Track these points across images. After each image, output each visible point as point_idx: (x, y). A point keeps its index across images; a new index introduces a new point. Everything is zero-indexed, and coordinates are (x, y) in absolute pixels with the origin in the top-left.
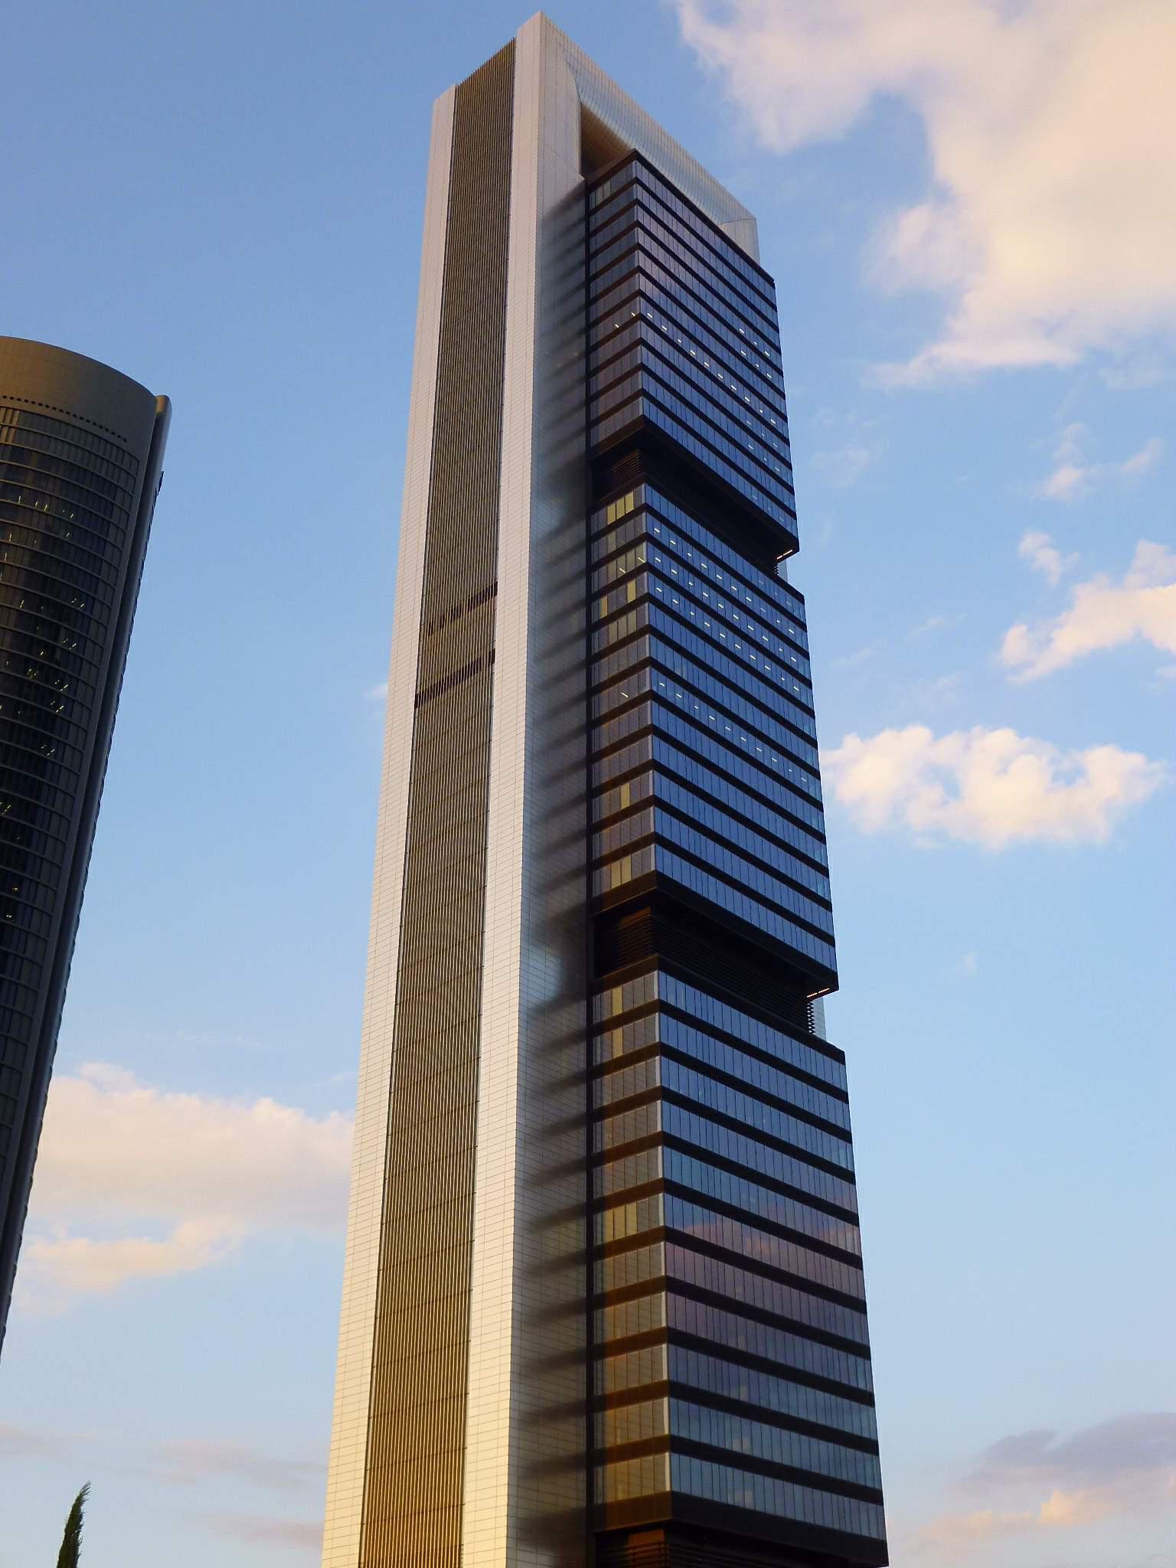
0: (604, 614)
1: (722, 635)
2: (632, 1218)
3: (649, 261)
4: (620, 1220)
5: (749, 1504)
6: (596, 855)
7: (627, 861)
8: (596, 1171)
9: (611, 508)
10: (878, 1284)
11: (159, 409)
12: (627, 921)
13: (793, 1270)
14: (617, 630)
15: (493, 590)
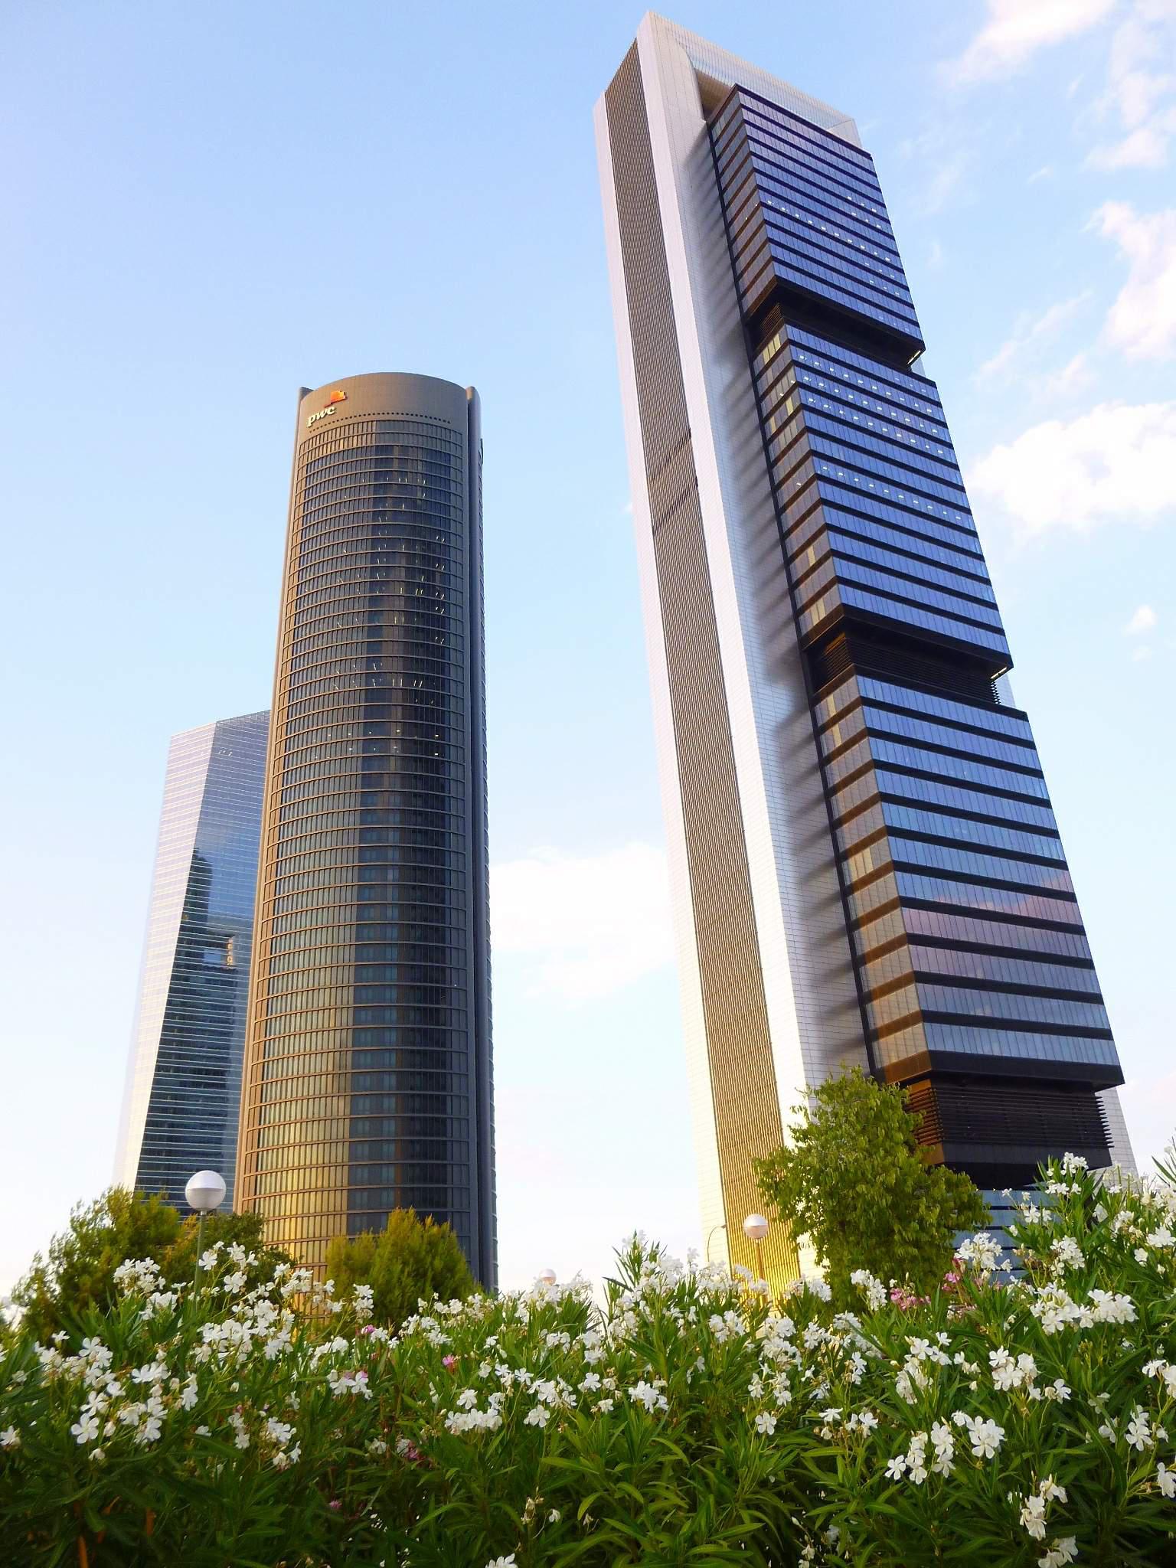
0: (774, 430)
1: (871, 424)
2: (869, 860)
3: (775, 231)
4: (860, 864)
5: (997, 1053)
6: (826, 753)
7: (820, 602)
8: (856, 933)
9: (765, 352)
10: (1090, 912)
11: (469, 397)
13: (1024, 947)
14: (783, 440)
15: (688, 434)
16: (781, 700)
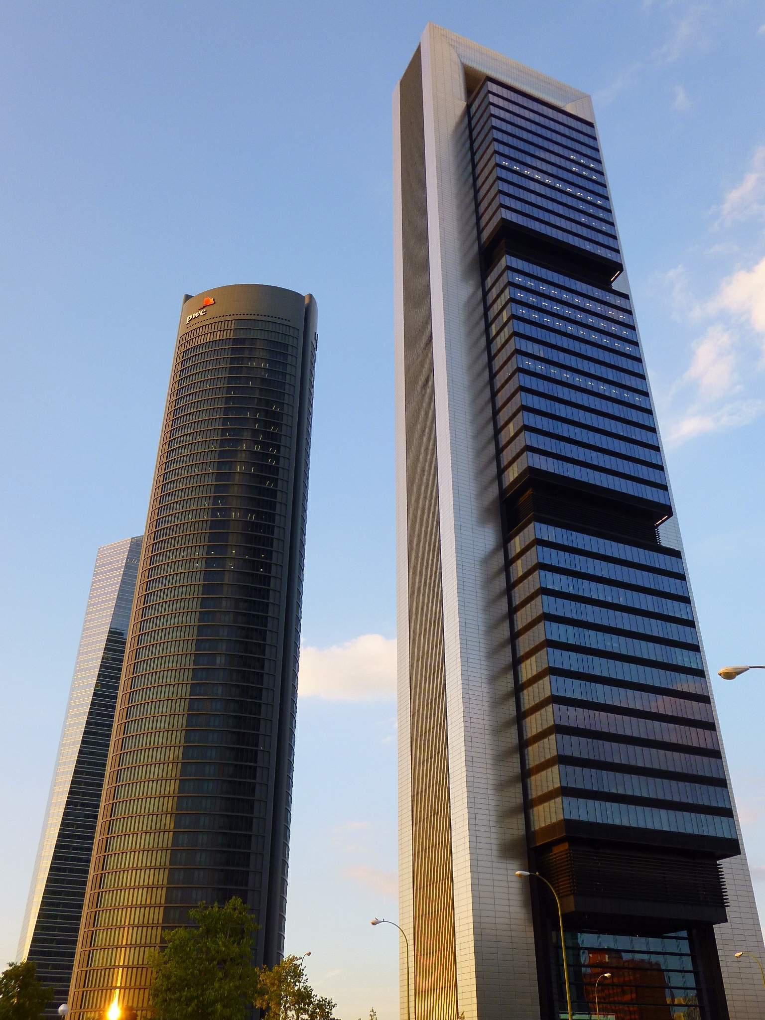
1: (570, 328)
4: (529, 667)
11: (307, 301)
12: (522, 499)
16: (486, 538)
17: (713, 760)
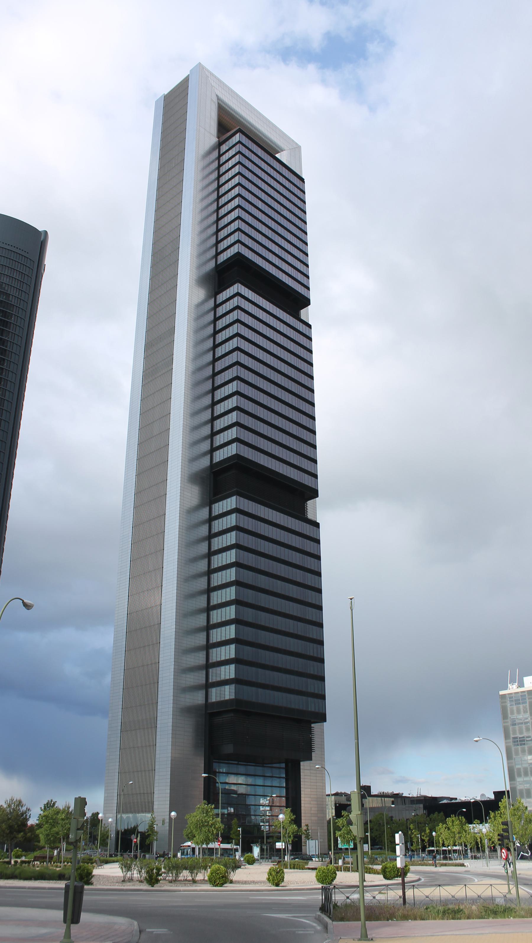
16: (194, 495)
17: (316, 577)
